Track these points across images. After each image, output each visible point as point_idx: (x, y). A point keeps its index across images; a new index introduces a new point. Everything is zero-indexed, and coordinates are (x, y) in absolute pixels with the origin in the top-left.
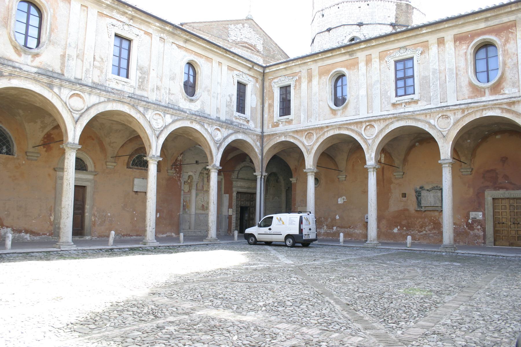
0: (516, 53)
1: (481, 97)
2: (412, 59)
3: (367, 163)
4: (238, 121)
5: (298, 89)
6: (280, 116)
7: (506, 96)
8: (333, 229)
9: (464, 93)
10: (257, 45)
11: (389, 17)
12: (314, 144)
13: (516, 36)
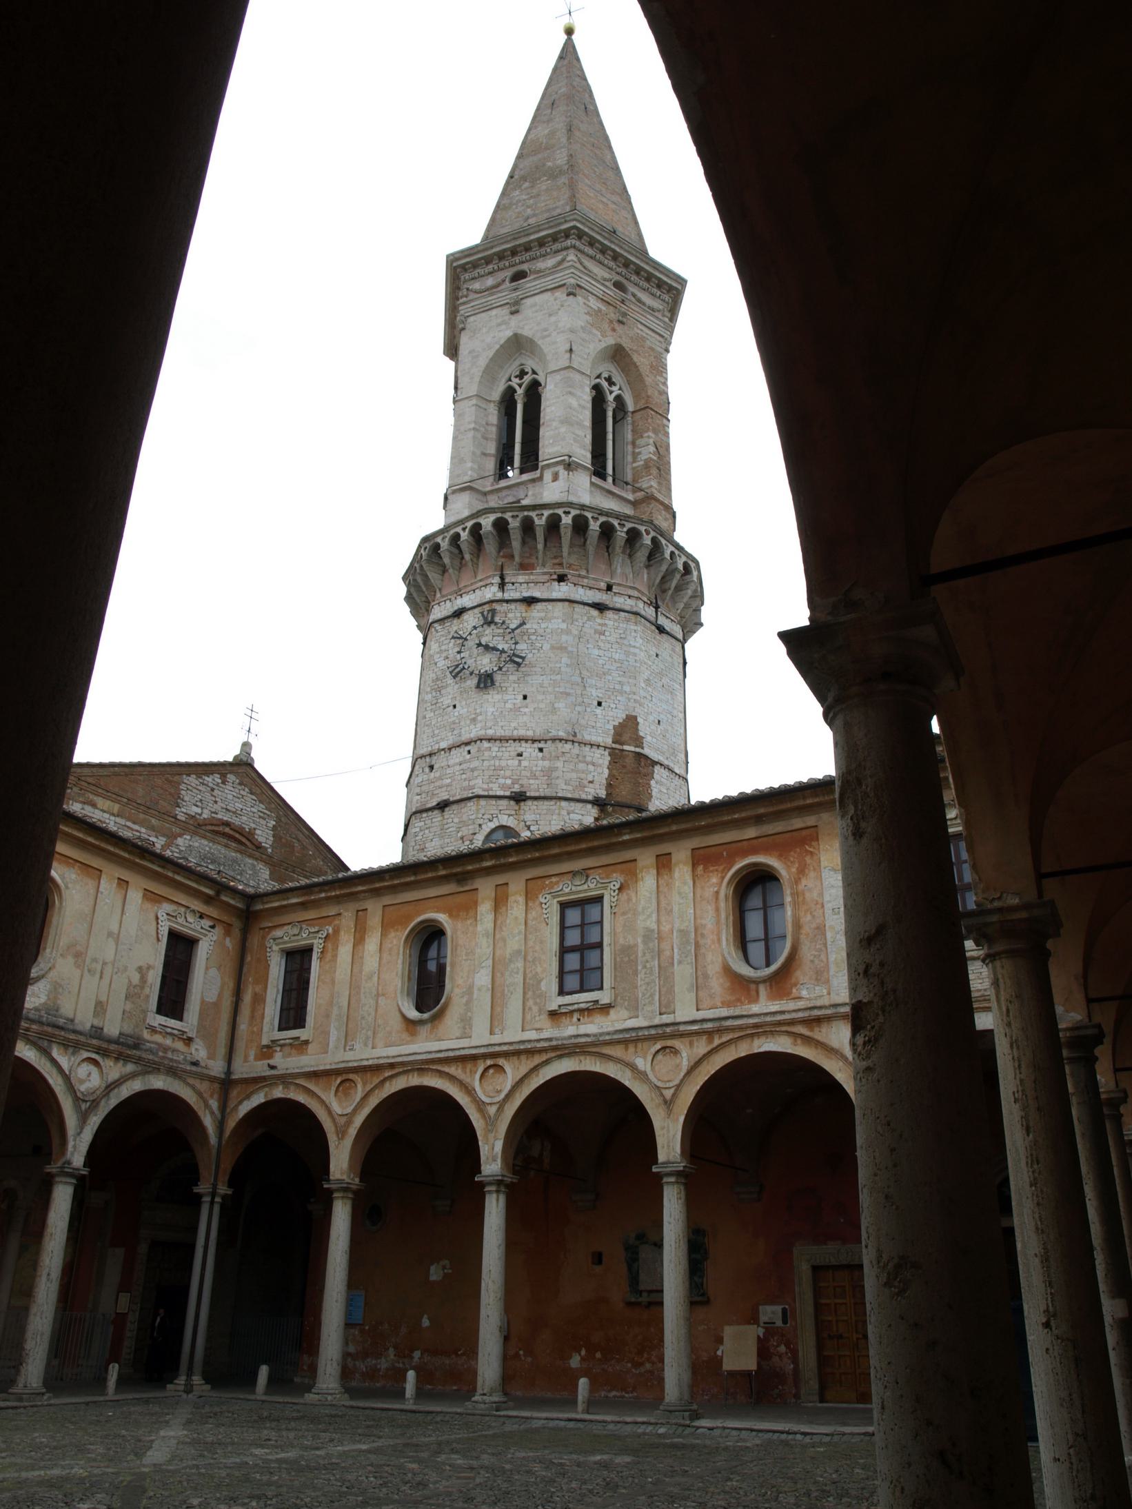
0: (820, 901)
1: (750, 1002)
2: (599, 899)
3: (482, 1168)
4: (158, 1038)
5: (330, 961)
6: (280, 1029)
7: (802, 1003)
8: (412, 1358)
9: (713, 991)
10: (258, 832)
11: (591, 782)
12: (355, 1111)
13: (820, 862)
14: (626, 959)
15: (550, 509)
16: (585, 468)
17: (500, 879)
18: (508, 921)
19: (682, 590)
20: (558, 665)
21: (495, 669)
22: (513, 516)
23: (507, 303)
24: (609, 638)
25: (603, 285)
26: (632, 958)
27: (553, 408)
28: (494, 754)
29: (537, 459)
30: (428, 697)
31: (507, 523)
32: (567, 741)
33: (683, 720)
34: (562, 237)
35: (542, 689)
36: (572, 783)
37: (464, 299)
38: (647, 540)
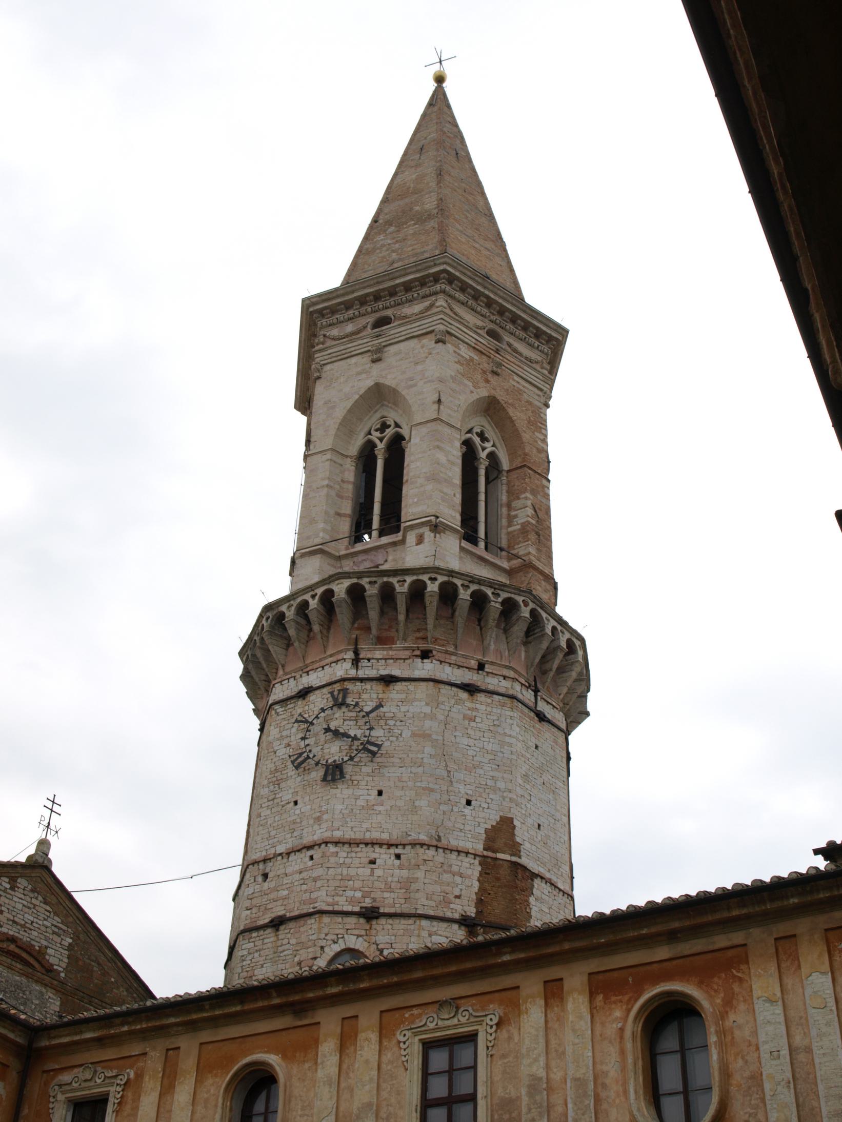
10: (50, 951)
13: (751, 991)
14: (506, 1117)
15: (414, 574)
16: (454, 530)
17: (348, 1010)
18: (357, 1066)
19: (563, 672)
20: (420, 756)
21: (346, 759)
22: (370, 583)
23: (369, 351)
24: (480, 725)
25: (475, 332)
26: (514, 1115)
27: (418, 464)
28: (341, 861)
29: (399, 519)
30: (265, 792)
31: (363, 589)
32: (429, 846)
33: (567, 826)
34: (431, 281)
35: (400, 784)
36: (435, 897)
37: (321, 346)
38: (525, 612)
